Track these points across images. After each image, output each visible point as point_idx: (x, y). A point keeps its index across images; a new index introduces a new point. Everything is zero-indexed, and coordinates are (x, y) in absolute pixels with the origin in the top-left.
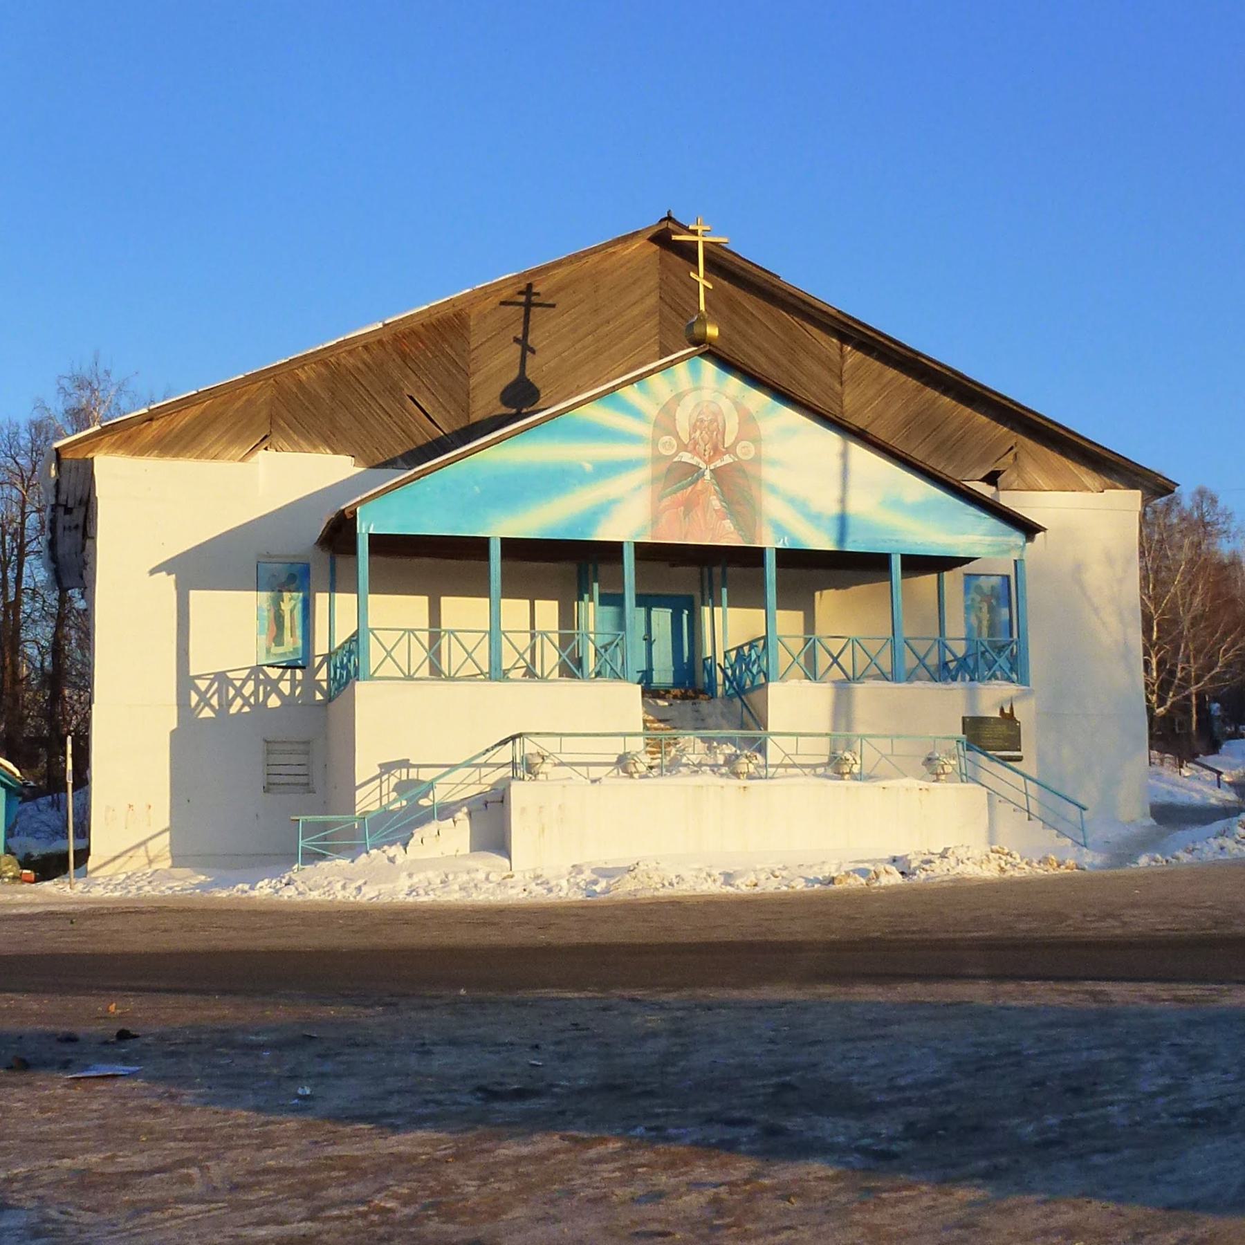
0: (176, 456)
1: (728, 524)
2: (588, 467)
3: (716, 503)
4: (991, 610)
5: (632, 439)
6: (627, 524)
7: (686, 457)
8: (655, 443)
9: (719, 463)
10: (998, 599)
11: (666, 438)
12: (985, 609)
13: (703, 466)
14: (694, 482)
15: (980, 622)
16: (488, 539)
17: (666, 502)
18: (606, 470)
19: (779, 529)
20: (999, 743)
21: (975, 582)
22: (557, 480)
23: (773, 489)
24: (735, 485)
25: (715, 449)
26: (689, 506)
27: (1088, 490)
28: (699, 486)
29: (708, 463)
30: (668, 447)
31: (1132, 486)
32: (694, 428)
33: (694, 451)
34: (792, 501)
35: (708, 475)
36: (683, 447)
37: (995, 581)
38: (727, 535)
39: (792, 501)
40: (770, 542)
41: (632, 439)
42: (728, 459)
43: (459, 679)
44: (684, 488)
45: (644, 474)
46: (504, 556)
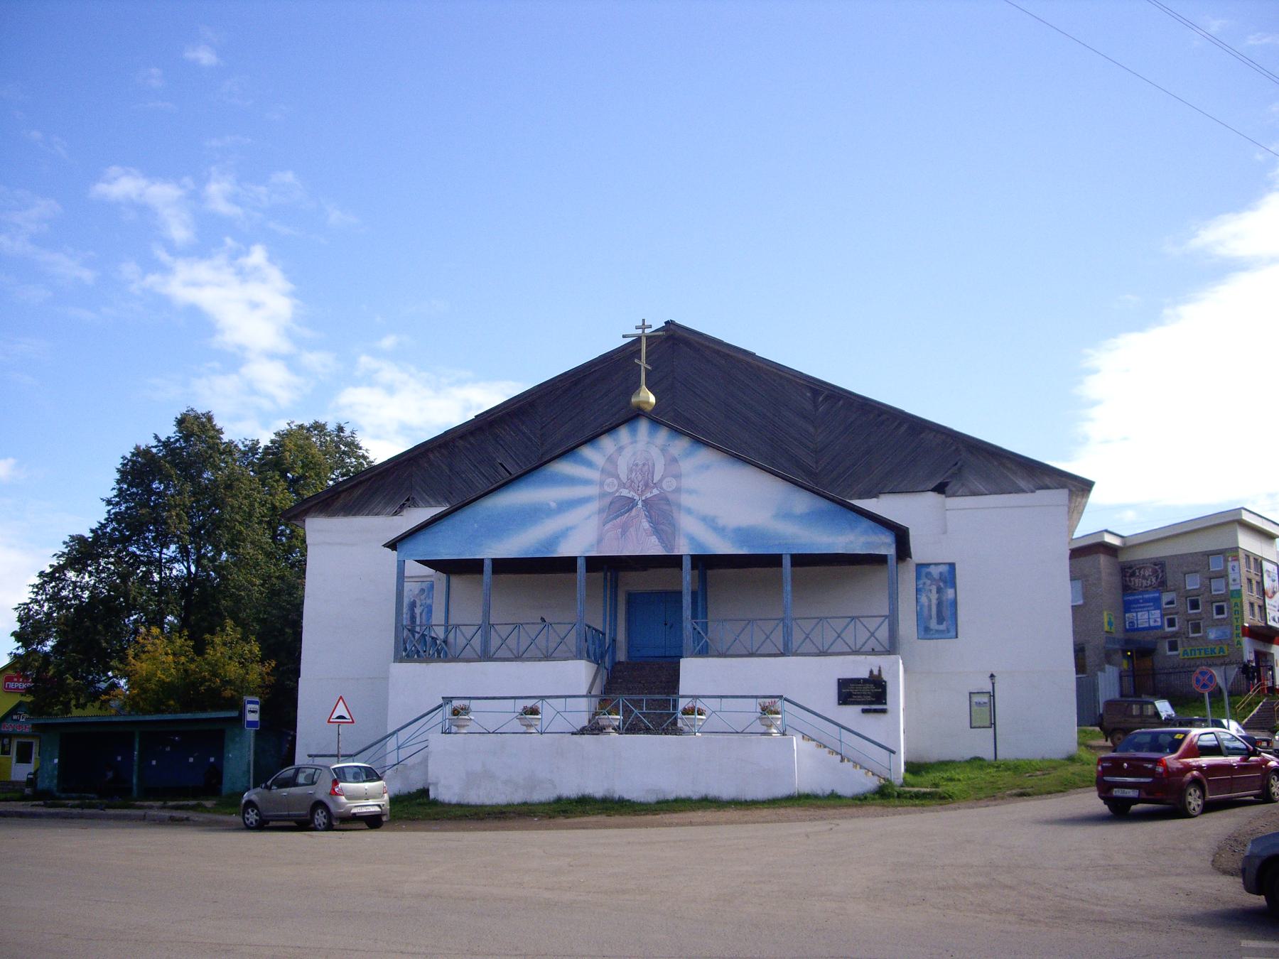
0: (354, 515)
1: (654, 539)
2: (553, 505)
3: (646, 525)
4: (939, 591)
5: (586, 482)
6: (576, 546)
7: (625, 492)
8: (602, 484)
9: (649, 495)
10: (945, 582)
11: (610, 480)
12: (934, 589)
13: (637, 498)
14: (630, 510)
15: (930, 600)
16: (780, 555)
17: (608, 526)
18: (566, 506)
19: (692, 539)
20: (869, 698)
21: (925, 570)
22: (534, 514)
23: (689, 511)
24: (660, 513)
25: (646, 485)
26: (624, 529)
27: (1023, 491)
28: (634, 512)
29: (640, 495)
30: (611, 486)
31: (1063, 487)
32: (631, 471)
33: (631, 487)
34: (704, 519)
35: (640, 504)
36: (623, 486)
37: (944, 569)
38: (653, 548)
39: (704, 519)
40: (683, 548)
41: (586, 482)
42: (655, 492)
43: (831, 654)
44: (622, 514)
45: (594, 506)
46: (693, 567)
